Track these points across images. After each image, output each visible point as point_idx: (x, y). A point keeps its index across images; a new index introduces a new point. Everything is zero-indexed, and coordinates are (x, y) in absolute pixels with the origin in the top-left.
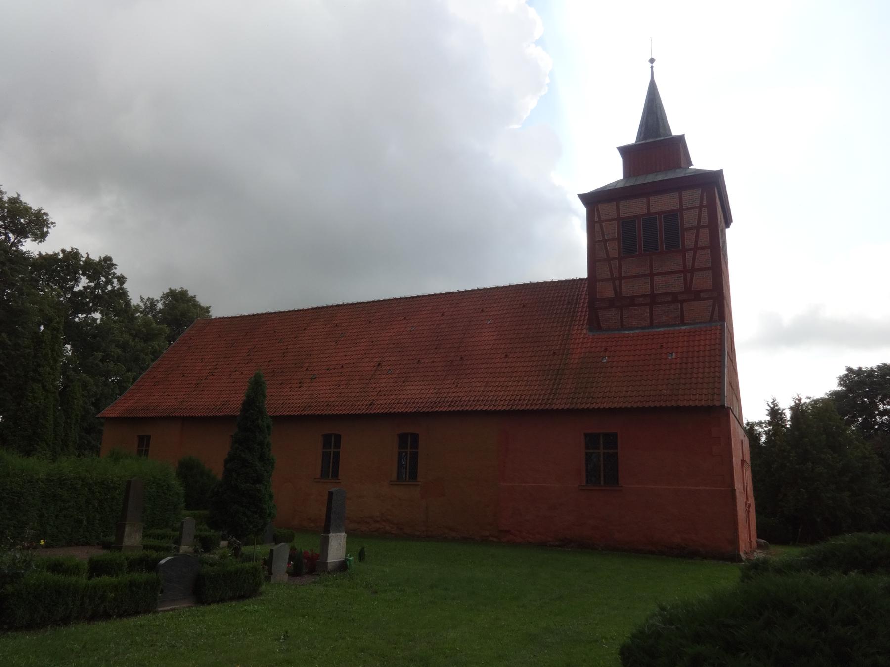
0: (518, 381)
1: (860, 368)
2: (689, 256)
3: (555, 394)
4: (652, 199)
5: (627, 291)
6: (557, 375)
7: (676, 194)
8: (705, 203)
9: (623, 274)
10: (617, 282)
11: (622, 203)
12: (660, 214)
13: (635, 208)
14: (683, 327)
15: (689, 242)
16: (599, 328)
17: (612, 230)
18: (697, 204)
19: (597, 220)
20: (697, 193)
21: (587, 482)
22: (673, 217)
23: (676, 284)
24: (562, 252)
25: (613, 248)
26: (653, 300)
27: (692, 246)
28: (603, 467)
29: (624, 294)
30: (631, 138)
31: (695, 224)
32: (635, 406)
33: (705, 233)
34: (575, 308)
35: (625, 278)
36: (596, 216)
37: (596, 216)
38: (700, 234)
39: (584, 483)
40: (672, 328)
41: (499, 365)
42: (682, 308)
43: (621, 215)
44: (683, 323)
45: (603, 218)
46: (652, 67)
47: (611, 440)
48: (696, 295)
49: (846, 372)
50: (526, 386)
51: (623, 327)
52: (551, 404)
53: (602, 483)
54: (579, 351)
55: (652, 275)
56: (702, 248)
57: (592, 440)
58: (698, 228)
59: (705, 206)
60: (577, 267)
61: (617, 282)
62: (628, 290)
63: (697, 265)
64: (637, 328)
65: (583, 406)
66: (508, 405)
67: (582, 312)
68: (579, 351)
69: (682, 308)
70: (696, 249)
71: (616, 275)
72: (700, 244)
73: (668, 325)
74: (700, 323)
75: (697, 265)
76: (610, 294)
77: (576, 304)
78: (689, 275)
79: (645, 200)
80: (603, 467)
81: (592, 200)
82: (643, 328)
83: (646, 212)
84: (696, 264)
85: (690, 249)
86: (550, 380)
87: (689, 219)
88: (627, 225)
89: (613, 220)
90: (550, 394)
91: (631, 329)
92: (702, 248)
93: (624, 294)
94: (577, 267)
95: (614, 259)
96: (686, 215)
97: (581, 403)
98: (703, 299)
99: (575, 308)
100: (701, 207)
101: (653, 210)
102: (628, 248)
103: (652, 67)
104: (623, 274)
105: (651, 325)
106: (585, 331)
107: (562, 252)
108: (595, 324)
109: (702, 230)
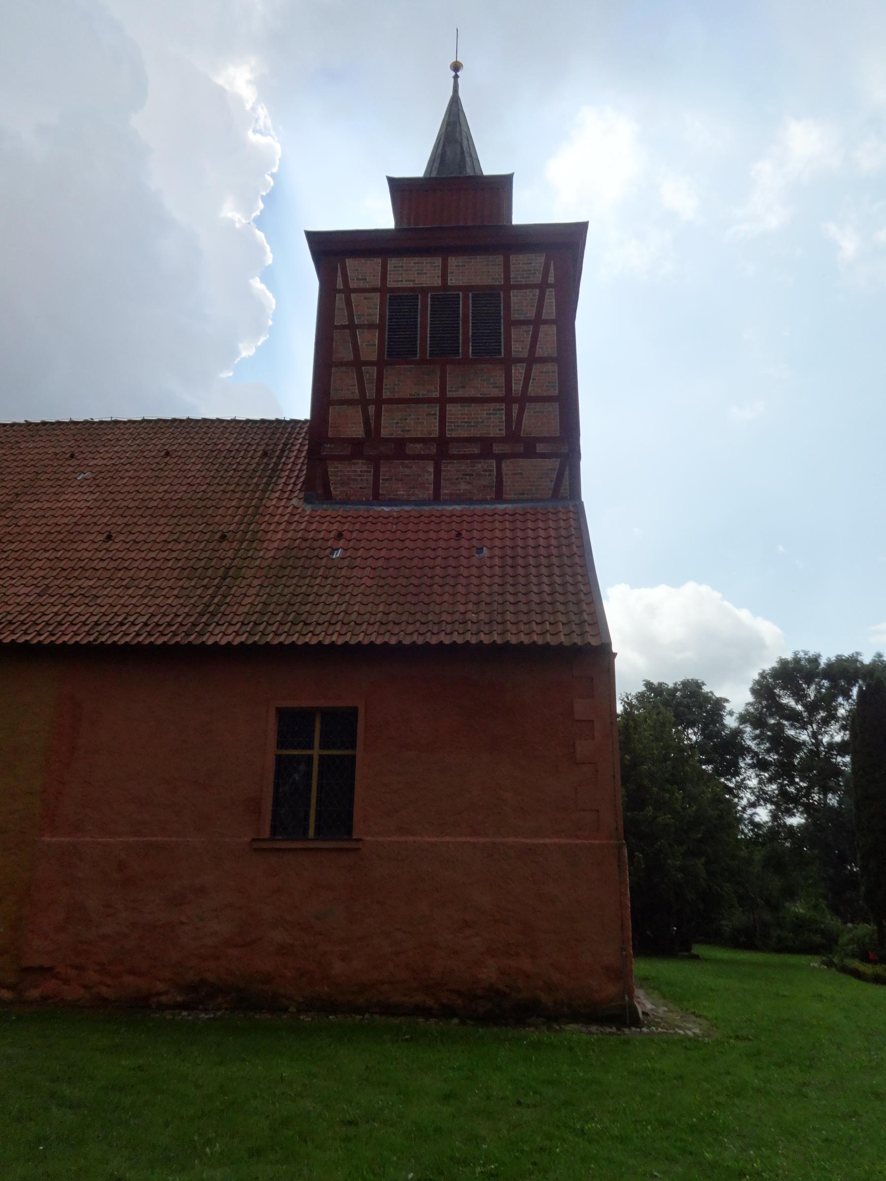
0: (127, 588)
1: (660, 684)
2: (518, 371)
3: (213, 614)
4: (453, 261)
5: (389, 427)
6: (224, 578)
7: (500, 259)
8: (551, 280)
9: (386, 394)
10: (372, 409)
11: (392, 263)
12: (466, 289)
13: (417, 273)
14: (501, 507)
15: (519, 348)
16: (327, 497)
17: (370, 309)
18: (537, 279)
19: (340, 285)
20: (538, 261)
21: (274, 829)
22: (490, 300)
23: (491, 422)
24: (265, 366)
25: (369, 344)
26: (442, 448)
27: (525, 354)
28: (313, 798)
29: (384, 433)
30: (415, 165)
31: (531, 314)
32: (407, 641)
33: (548, 334)
34: (276, 464)
35: (391, 401)
36: (339, 279)
37: (339, 279)
38: (541, 335)
39: (266, 833)
40: (479, 507)
41: (87, 555)
42: (499, 469)
43: (390, 284)
44: (499, 498)
45: (353, 285)
46: (456, 77)
47: (341, 725)
48: (529, 448)
49: (644, 689)
50: (143, 597)
51: (377, 498)
52: (200, 634)
53: (311, 833)
54: (279, 535)
55: (443, 401)
56: (543, 360)
57: (293, 725)
58: (537, 322)
59: (551, 286)
60: (293, 399)
61: (372, 409)
62: (391, 425)
63: (532, 391)
64: (407, 502)
65: (282, 638)
66: (88, 634)
67: (292, 471)
68: (279, 535)
69: (499, 469)
70: (532, 360)
71: (371, 393)
72: (539, 352)
73: (471, 501)
74: (531, 500)
75: (532, 391)
76: (356, 430)
77: (280, 457)
78: (515, 408)
79: (438, 261)
80: (313, 798)
81: (332, 251)
82: (423, 502)
83: (438, 282)
84: (530, 389)
85: (521, 361)
86: (206, 587)
87: (521, 304)
88: (400, 304)
89: (374, 290)
90: (201, 614)
91: (391, 502)
92: (543, 360)
93: (384, 433)
94: (293, 399)
95: (370, 363)
96: (515, 297)
97: (276, 634)
98: (543, 456)
99: (276, 464)
100: (543, 286)
101: (452, 281)
102: (399, 346)
103: (456, 77)
104: (386, 394)
105: (437, 498)
106: (294, 502)
107: (265, 366)
108: (317, 488)
109: (543, 328)
